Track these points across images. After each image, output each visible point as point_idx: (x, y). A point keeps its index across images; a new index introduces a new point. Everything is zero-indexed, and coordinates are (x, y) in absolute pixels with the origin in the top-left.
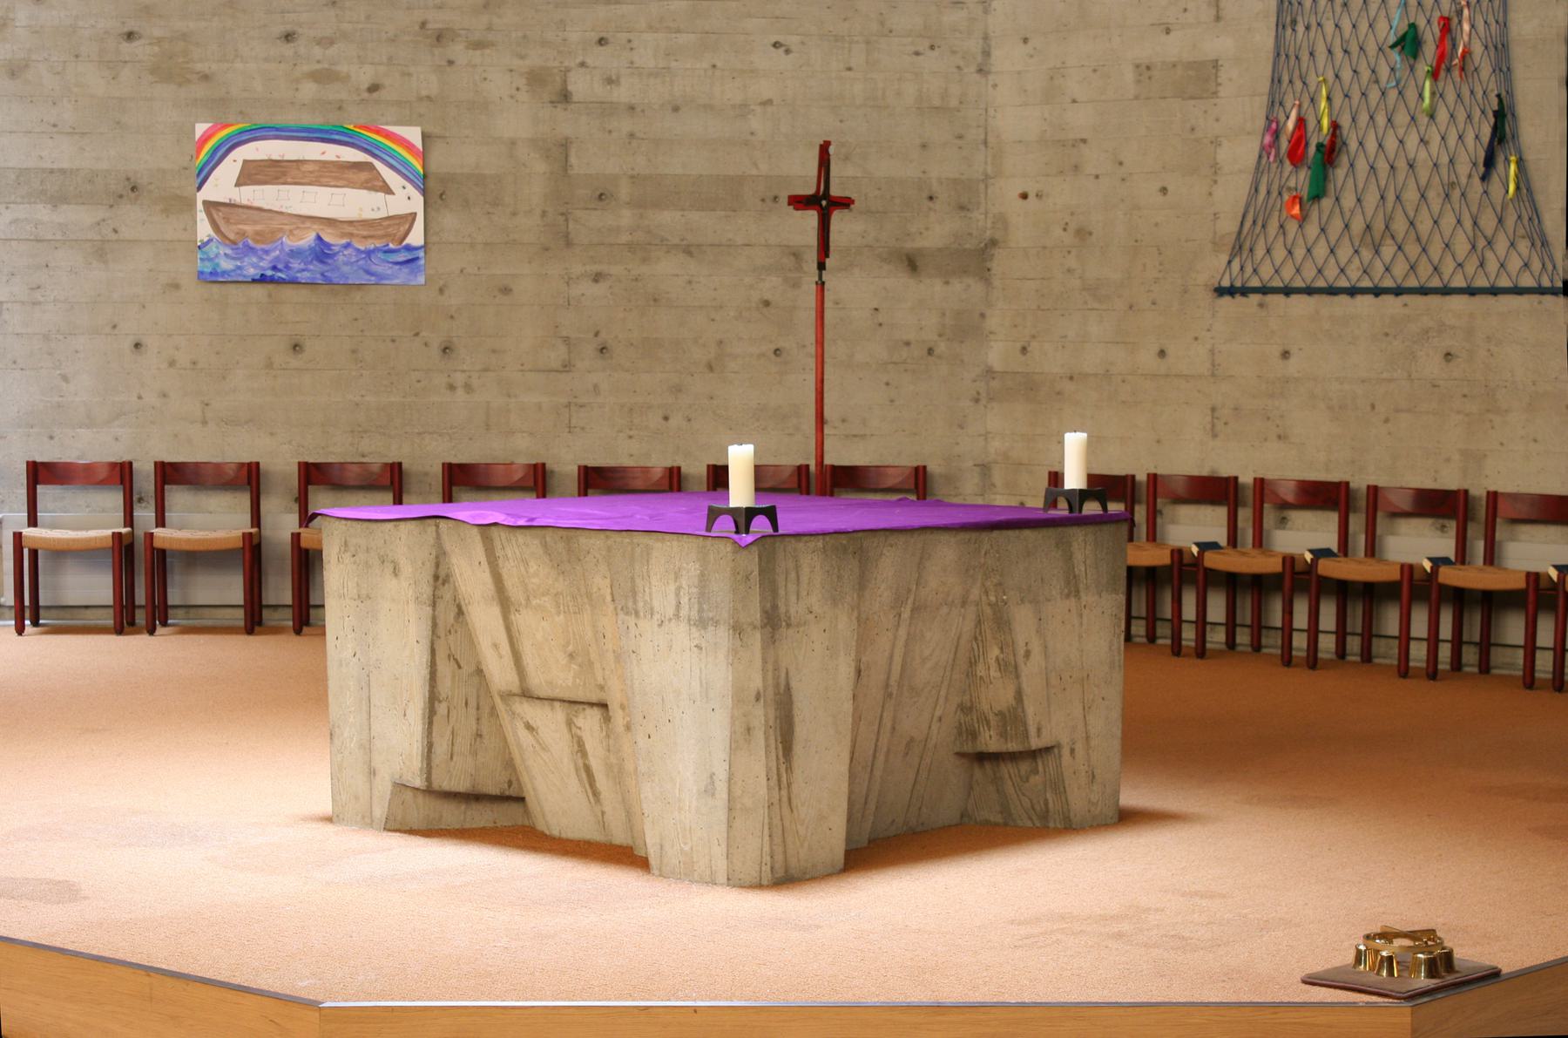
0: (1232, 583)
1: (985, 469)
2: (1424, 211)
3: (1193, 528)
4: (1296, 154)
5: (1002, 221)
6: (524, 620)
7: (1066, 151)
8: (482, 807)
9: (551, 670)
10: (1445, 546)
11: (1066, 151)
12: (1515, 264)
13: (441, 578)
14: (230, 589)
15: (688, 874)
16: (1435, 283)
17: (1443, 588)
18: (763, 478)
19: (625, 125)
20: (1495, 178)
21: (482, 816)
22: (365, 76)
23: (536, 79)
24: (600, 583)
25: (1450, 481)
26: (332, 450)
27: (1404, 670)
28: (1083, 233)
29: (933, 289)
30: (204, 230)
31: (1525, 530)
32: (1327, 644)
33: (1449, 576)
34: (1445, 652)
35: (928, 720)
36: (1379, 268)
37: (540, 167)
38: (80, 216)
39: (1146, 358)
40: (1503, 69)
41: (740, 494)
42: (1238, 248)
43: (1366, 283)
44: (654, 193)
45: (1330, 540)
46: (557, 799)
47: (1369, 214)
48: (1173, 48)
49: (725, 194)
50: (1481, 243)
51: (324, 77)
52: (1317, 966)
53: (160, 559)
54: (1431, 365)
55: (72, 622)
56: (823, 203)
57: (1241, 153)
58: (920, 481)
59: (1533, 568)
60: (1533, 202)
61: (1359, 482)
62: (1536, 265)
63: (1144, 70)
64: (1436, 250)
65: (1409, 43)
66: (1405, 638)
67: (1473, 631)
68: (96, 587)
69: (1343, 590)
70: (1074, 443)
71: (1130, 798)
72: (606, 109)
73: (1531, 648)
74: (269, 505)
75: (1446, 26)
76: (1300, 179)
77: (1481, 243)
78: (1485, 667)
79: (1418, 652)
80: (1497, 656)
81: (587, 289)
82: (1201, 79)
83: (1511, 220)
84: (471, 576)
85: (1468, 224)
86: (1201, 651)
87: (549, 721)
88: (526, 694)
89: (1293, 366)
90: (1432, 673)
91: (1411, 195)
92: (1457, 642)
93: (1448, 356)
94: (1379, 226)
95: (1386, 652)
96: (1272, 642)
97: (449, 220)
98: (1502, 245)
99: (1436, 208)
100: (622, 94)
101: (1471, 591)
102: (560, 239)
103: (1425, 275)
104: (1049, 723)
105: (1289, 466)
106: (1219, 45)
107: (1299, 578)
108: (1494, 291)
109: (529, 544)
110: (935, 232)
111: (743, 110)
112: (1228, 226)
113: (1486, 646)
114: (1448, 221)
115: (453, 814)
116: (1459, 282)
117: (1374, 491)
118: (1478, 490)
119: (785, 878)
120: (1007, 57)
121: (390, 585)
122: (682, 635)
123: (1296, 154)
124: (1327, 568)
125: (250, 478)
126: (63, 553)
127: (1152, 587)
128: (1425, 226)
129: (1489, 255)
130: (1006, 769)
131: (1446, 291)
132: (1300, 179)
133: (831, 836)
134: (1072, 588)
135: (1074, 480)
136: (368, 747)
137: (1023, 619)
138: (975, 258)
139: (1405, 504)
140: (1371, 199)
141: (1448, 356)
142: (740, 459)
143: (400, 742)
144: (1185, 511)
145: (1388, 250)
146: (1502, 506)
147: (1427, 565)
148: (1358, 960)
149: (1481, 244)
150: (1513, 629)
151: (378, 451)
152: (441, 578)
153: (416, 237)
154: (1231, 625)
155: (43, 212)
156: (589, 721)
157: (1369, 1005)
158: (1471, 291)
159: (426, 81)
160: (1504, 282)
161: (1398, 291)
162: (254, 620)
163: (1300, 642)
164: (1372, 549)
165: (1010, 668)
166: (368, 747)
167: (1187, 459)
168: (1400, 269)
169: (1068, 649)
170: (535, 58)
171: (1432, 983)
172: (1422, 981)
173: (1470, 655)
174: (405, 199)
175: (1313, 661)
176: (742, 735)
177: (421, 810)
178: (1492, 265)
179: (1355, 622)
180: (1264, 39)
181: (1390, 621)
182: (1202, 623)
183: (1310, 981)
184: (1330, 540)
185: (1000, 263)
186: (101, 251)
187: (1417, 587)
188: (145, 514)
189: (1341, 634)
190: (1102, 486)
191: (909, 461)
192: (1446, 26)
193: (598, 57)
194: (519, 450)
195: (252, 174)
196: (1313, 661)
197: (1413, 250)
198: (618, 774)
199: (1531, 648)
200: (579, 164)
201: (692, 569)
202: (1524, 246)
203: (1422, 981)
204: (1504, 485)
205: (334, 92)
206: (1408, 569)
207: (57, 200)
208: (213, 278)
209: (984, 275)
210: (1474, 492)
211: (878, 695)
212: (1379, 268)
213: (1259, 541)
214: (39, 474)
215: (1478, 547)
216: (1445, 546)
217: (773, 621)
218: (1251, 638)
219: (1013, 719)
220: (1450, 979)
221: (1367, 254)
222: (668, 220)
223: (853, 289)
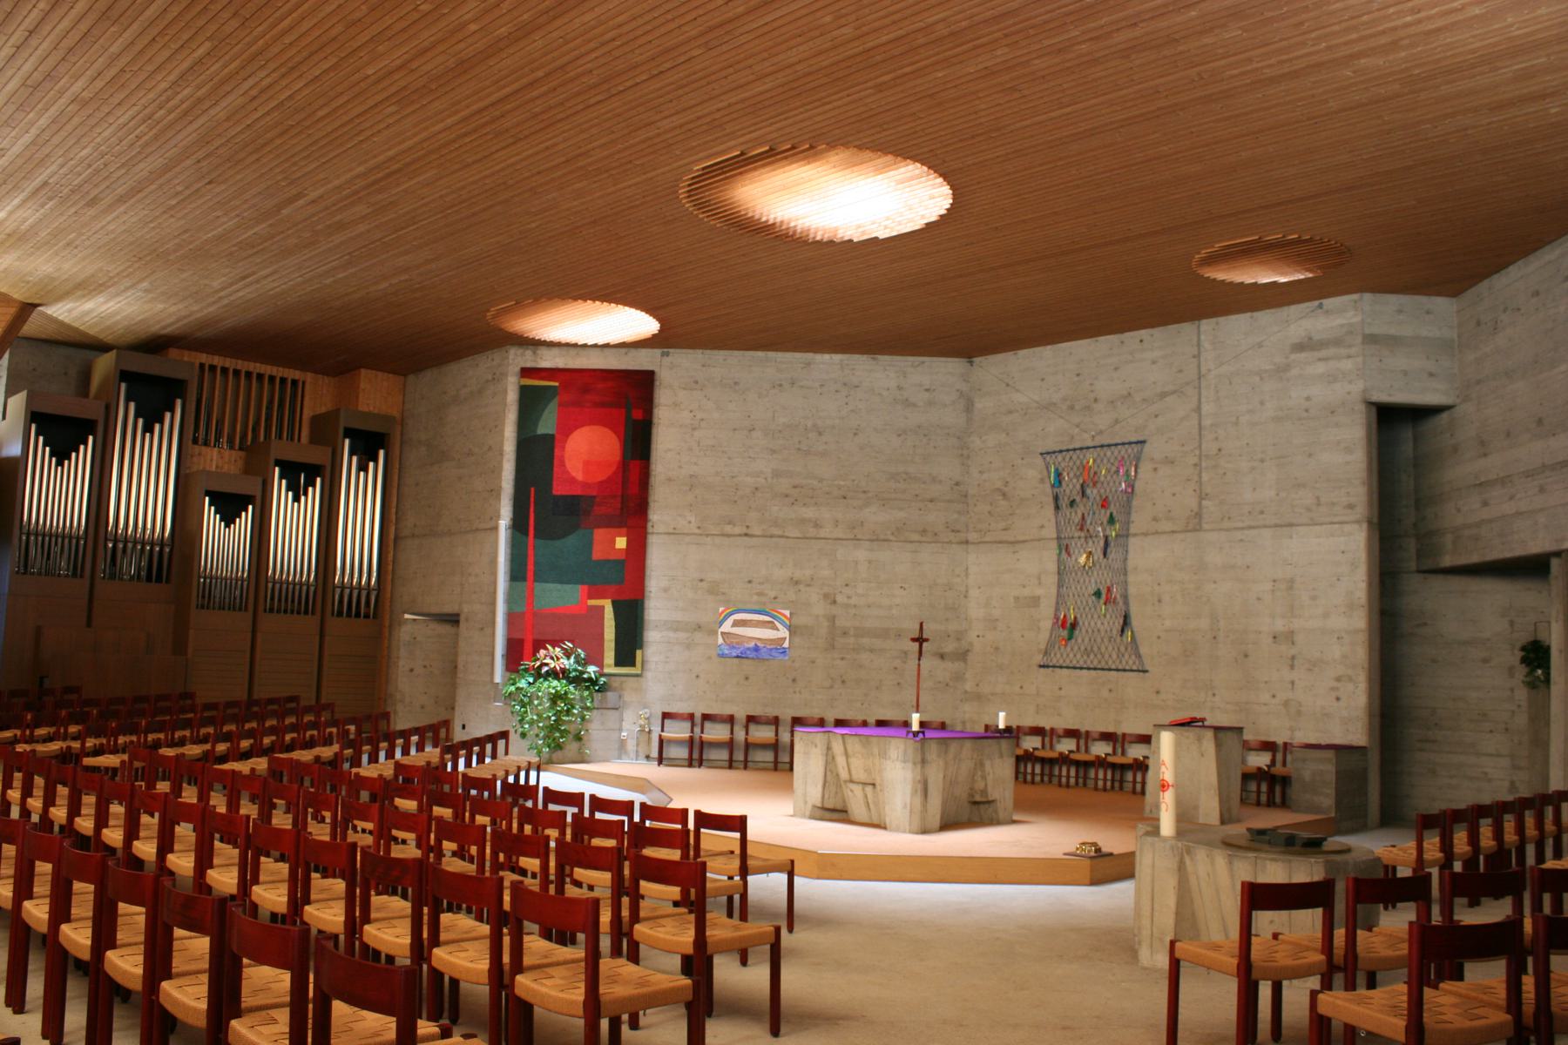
0: (1043, 761)
1: (964, 723)
3: (1030, 743)
4: (1063, 626)
5: (971, 644)
6: (852, 760)
7: (992, 623)
8: (836, 812)
9: (860, 775)
10: (1109, 750)
11: (992, 623)
13: (829, 748)
14: (723, 755)
15: (897, 830)
18: (922, 724)
19: (853, 611)
21: (836, 815)
22: (772, 594)
23: (826, 596)
24: (876, 751)
25: (1111, 729)
26: (757, 711)
27: (1096, 789)
28: (997, 649)
29: (949, 665)
30: (720, 640)
32: (1072, 781)
33: (1110, 759)
35: (961, 792)
37: (826, 624)
38: (682, 635)
39: (1017, 689)
40: (1126, 603)
41: (915, 727)
42: (1046, 653)
44: (861, 632)
45: (1074, 747)
46: (857, 809)
48: (1027, 592)
49: (884, 634)
51: (760, 594)
53: (702, 743)
54: (1105, 693)
55: (673, 763)
56: (920, 640)
57: (1047, 624)
58: (943, 726)
61: (1083, 730)
63: (1017, 599)
65: (1098, 594)
66: (1096, 779)
67: (1118, 777)
68: (683, 753)
69: (1078, 763)
70: (1002, 715)
71: (1015, 818)
72: (847, 606)
74: (736, 728)
75: (1109, 590)
76: (1065, 633)
79: (1100, 783)
81: (838, 662)
82: (1035, 601)
84: (837, 747)
86: (1033, 782)
87: (857, 789)
88: (852, 781)
89: (1063, 693)
90: (1105, 789)
92: (1113, 780)
95: (1091, 783)
96: (1055, 780)
97: (797, 640)
100: (853, 601)
102: (831, 646)
103: (1103, 665)
104: (994, 794)
105: (1061, 724)
106: (1039, 592)
107: (1064, 759)
109: (856, 739)
110: (949, 647)
111: (890, 608)
112: (1043, 647)
113: (1122, 781)
115: (828, 815)
119: (924, 832)
120: (974, 593)
121: (814, 750)
122: (899, 765)
123: (1063, 626)
124: (1073, 756)
125: (731, 720)
126: (671, 741)
127: (1023, 759)
130: (982, 807)
132: (1065, 633)
133: (936, 820)
134: (1001, 756)
135: (1002, 726)
136: (805, 795)
137: (988, 764)
138: (962, 655)
142: (915, 719)
143: (814, 794)
144: (1028, 738)
149: (1120, 655)
151: (771, 712)
152: (829, 748)
153: (786, 645)
154: (1042, 775)
155: (671, 634)
156: (869, 789)
159: (791, 595)
162: (731, 765)
163: (1064, 780)
164: (1087, 751)
165: (984, 778)
166: (805, 795)
167: (1029, 721)
169: (999, 771)
170: (826, 590)
173: (1117, 785)
174: (783, 633)
175: (1068, 786)
176: (914, 792)
177: (819, 813)
179: (1081, 774)
180: (1054, 590)
181: (1092, 773)
182: (1033, 774)
184: (1074, 747)
185: (970, 657)
186: (688, 646)
187: (1100, 762)
188: (697, 730)
189: (1077, 777)
190: (1008, 729)
191: (775, 713)
192: (1109, 590)
193: (847, 591)
194: (815, 713)
195: (736, 624)
196: (1068, 786)
198: (876, 804)
200: (838, 623)
201: (902, 747)
204: (1128, 731)
205: (763, 599)
206: (1098, 757)
207: (676, 630)
208: (722, 656)
209: (965, 661)
211: (950, 784)
213: (1052, 747)
214: (666, 716)
215: (1119, 751)
216: (1109, 750)
217: (923, 762)
218: (1048, 778)
219: (984, 792)
222: (865, 641)
223: (926, 663)
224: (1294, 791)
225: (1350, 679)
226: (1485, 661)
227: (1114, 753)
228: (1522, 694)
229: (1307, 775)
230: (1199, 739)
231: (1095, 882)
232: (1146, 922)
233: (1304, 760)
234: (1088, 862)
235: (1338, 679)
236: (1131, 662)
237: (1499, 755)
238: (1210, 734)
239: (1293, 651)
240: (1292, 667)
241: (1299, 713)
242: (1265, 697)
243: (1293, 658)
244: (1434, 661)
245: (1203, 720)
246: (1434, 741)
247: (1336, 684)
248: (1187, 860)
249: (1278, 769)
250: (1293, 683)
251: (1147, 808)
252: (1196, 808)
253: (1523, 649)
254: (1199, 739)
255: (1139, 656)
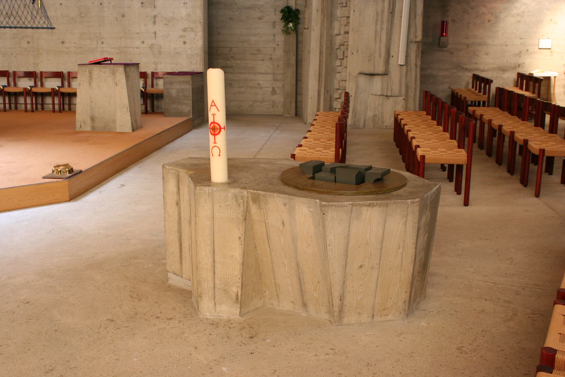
2: (20, 11)
12: (42, 22)
16: (24, 26)
17: (6, 92)
20: (35, 4)
25: (31, 69)
27: (26, 111)
31: (49, 79)
34: (7, 106)
36: (10, 22)
43: (7, 26)
47: (7, 10)
50: (34, 17)
52: (44, 175)
54: (25, 45)
59: (25, 87)
60: (45, 9)
62: (47, 23)
64: (23, 19)
67: (40, 101)
73: (26, 104)
77: (34, 17)
78: (43, 109)
79: (29, 107)
80: (19, 106)
83: (40, 12)
85: (30, 13)
90: (33, 111)
91: (16, 7)
93: (28, 42)
94: (9, 13)
98: (38, 18)
99: (22, 9)
101: (38, 93)
103: (21, 24)
108: (38, 28)
114: (26, 12)
116: (29, 26)
117: (14, 72)
118: (38, 71)
128: (20, 13)
129: (36, 20)
131: (26, 28)
139: (22, 75)
140: (7, 7)
141: (28, 42)
145: (12, 18)
146: (44, 75)
147: (29, 88)
148: (53, 171)
149: (33, 18)
150: (49, 100)
157: (56, 182)
158: (32, 28)
160: (40, 26)
161: (15, 28)
164: (15, 85)
168: (15, 23)
171: (70, 175)
172: (68, 175)
173: (39, 107)
178: (37, 23)
179: (13, 101)
183: (44, 178)
187: (27, 93)
197: (18, 19)
199: (54, 104)
202: (43, 18)
203: (68, 175)
204: (44, 70)
210: (37, 72)
212: (10, 22)
215: (39, 83)
216: (32, 83)
220: (73, 173)
221: (7, 19)
224: (163, 104)
225: (192, 29)
226: (260, 18)
227: (36, 85)
228: (280, 38)
229: (174, 93)
230: (114, 73)
231: (73, 197)
232: (206, 274)
233: (172, 83)
234: (66, 182)
235: (185, 30)
236: (42, 22)
237: (267, 73)
238: (121, 69)
239: (154, 13)
240: (154, 23)
241: (160, 53)
242: (138, 43)
243: (155, 17)
244: (231, 19)
245: (111, 59)
246: (231, 67)
247: (184, 34)
248: (254, 209)
249: (66, 90)
250: (155, 33)
251: (78, 125)
252: (114, 121)
253: (282, 11)
254: (114, 73)
255: (47, 18)
